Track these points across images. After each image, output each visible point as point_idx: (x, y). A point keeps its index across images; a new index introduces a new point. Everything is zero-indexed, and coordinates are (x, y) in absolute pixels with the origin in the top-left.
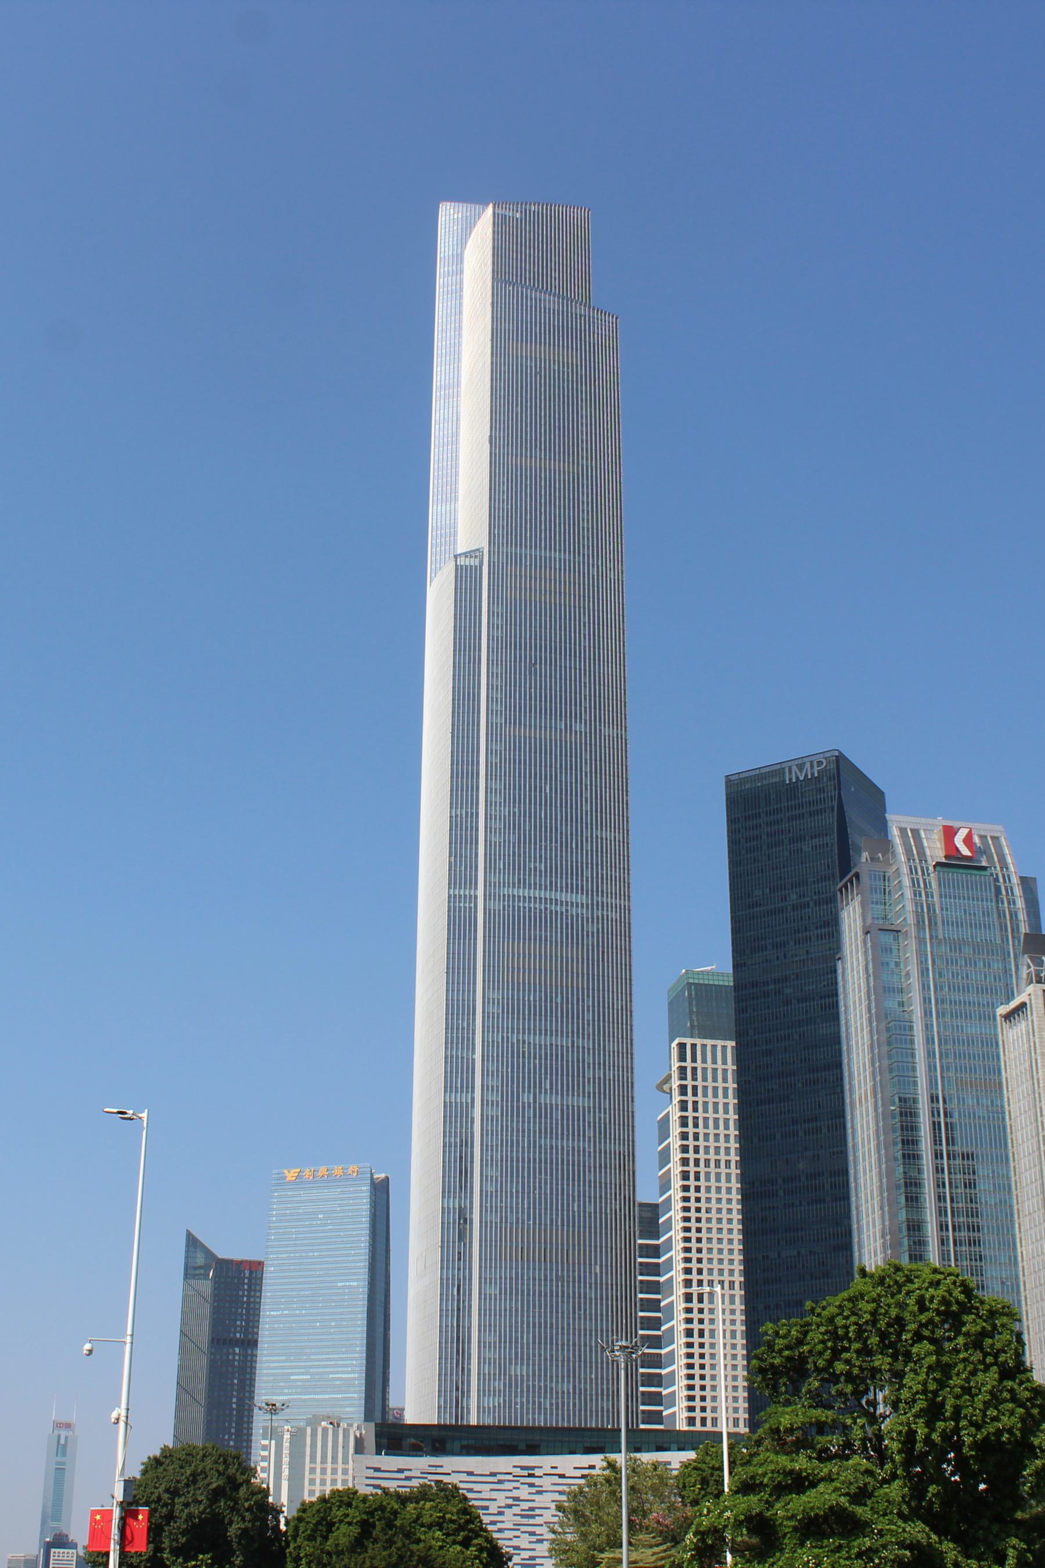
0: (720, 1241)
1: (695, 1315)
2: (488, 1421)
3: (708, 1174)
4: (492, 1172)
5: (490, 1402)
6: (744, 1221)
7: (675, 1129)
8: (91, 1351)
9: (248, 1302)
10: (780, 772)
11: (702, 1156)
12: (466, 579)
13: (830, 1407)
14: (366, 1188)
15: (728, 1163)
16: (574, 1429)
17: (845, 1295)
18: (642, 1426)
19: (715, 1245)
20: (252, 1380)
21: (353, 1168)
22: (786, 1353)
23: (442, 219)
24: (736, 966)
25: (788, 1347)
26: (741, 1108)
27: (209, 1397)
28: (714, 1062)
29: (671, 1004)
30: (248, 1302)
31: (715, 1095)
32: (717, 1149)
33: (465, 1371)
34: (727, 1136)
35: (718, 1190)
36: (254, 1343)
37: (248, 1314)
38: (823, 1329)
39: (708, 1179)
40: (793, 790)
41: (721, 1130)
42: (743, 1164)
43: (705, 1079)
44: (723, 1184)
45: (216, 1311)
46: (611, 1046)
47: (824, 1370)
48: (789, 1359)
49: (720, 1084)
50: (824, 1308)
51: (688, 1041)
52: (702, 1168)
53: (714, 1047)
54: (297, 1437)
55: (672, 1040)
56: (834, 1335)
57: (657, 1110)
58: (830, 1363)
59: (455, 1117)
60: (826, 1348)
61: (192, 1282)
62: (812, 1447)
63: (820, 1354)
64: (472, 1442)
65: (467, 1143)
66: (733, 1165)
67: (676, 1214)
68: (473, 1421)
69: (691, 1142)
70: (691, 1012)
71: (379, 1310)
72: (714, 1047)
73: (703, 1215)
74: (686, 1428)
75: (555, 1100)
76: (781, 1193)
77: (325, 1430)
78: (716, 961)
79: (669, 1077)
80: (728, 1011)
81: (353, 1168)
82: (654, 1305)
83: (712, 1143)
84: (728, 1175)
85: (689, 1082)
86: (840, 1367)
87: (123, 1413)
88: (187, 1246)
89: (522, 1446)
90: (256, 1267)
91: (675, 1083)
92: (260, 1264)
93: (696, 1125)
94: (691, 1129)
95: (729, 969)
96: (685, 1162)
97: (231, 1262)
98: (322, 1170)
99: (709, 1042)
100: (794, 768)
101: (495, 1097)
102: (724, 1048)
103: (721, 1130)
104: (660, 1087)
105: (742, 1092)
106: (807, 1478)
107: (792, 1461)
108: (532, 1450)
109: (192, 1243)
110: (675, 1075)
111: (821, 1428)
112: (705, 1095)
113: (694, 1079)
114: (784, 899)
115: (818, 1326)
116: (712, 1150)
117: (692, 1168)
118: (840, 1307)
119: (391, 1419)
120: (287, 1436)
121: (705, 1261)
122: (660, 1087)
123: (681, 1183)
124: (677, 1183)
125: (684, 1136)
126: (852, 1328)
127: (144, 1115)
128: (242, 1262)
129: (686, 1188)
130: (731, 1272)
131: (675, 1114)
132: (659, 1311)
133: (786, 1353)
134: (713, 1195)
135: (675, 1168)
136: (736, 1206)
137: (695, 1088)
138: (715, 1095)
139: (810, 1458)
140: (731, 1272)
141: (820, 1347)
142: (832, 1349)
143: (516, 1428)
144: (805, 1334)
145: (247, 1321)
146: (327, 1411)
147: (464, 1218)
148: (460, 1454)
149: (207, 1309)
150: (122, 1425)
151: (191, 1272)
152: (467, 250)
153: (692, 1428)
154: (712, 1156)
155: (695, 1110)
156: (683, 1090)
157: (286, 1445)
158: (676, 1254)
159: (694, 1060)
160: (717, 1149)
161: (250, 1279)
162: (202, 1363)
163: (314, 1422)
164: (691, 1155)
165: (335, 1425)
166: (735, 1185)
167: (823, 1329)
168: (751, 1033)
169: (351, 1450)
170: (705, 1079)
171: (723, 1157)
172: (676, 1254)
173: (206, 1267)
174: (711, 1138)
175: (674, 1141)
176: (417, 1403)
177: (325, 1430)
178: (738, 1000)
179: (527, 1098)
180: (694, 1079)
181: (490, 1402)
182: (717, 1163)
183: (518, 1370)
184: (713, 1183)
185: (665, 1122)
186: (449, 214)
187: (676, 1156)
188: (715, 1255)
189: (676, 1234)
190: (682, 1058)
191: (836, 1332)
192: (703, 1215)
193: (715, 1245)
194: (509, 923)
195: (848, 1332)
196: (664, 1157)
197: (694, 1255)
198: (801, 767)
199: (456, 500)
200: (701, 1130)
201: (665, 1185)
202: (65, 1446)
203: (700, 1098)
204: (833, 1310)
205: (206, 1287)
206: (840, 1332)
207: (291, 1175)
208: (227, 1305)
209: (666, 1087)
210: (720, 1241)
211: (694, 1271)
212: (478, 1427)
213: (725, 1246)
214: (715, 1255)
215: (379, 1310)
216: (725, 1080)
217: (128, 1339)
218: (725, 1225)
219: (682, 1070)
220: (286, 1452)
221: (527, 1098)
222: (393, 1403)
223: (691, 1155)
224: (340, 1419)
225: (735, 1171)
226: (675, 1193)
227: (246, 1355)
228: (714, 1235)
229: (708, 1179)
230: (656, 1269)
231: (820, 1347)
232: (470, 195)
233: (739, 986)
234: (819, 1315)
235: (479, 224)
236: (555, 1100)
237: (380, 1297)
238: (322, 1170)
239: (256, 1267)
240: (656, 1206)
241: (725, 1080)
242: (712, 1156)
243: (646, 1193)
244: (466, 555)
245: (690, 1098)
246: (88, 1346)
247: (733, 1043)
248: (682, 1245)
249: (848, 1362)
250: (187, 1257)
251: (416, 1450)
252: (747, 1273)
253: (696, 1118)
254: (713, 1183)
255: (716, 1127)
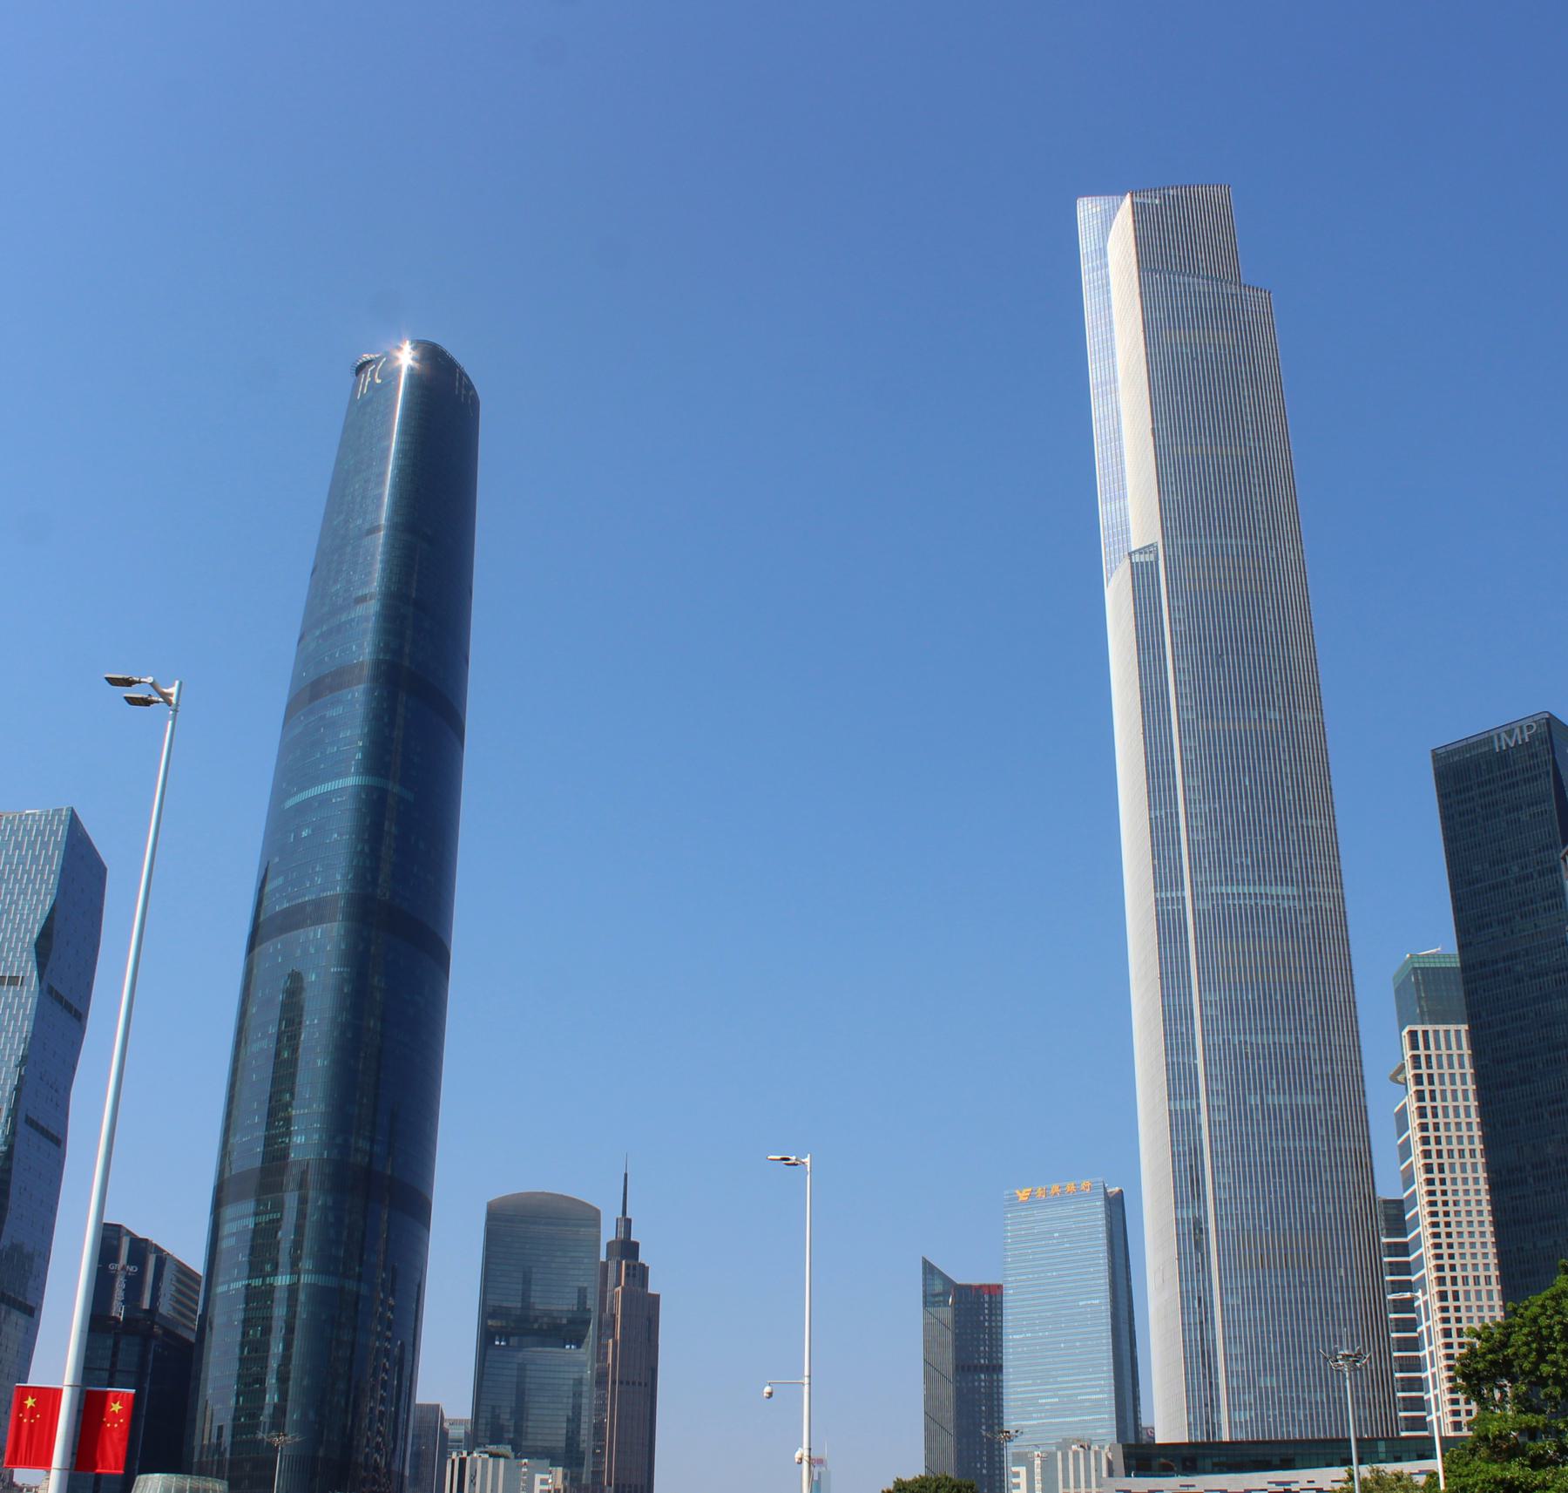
0: (1471, 1234)
1: (1452, 1314)
2: (1241, 1436)
3: (1452, 1166)
4: (1225, 1179)
5: (1242, 1416)
6: (1493, 1212)
7: (1414, 1121)
8: (770, 1394)
9: (990, 1327)
10: (1490, 740)
11: (1444, 1147)
12: (1142, 576)
13: (1539, 1411)
14: (1100, 1203)
15: (1472, 1152)
16: (1332, 1440)
17: (1547, 1293)
18: (1403, 1434)
19: (1466, 1239)
20: (1000, 1406)
21: (1085, 1184)
22: (1490, 1357)
23: (1080, 215)
24: (1461, 947)
25: (1491, 1351)
26: (1480, 1094)
27: (957, 1426)
28: (1449, 1047)
29: (1398, 992)
30: (990, 1327)
31: (1453, 1082)
32: (1460, 1138)
33: (1213, 1385)
34: (1469, 1125)
35: (1465, 1181)
36: (999, 1369)
37: (991, 1339)
38: (1525, 1330)
39: (1452, 1170)
40: (1504, 757)
41: (1463, 1119)
42: (1487, 1152)
43: (1440, 1066)
44: (1470, 1174)
45: (958, 1337)
46: (1336, 1040)
47: (1531, 1372)
48: (1493, 1363)
49: (1457, 1070)
50: (1526, 1308)
51: (1419, 1028)
52: (1445, 1160)
53: (1447, 1032)
54: (1049, 1462)
55: (1402, 1029)
56: (1538, 1336)
57: (1391, 1102)
58: (1536, 1365)
59: (1181, 1124)
60: (1530, 1352)
61: (931, 1310)
62: (1524, 1454)
63: (1526, 1356)
64: (1223, 1459)
65: (1197, 1152)
66: (1478, 1153)
67: (1422, 1209)
68: (1226, 1437)
69: (1431, 1133)
70: (1419, 998)
71: (1125, 1328)
72: (1447, 1032)
73: (1451, 1208)
74: (1452, 1434)
75: (1283, 1100)
76: (1531, 1180)
77: (1076, 1454)
78: (1440, 943)
79: (1403, 1067)
80: (1457, 995)
81: (1085, 1184)
82: (1408, 1306)
83: (1453, 1133)
84: (1474, 1165)
85: (1424, 1071)
86: (1546, 1369)
87: (806, 1453)
88: (925, 1273)
89: (1276, 1461)
90: (995, 1291)
91: (1410, 1073)
92: (1000, 1287)
93: (1435, 1115)
94: (1430, 1120)
95: (1455, 950)
96: (1427, 1154)
97: (970, 1287)
98: (1055, 1188)
99: (1441, 1028)
100: (1503, 736)
101: (1222, 1102)
102: (1458, 1032)
103: (1463, 1119)
104: (1394, 1078)
105: (1479, 1078)
106: (1519, 1487)
107: (1504, 1469)
108: (1287, 1464)
109: (929, 1269)
110: (1409, 1065)
111: (1532, 1433)
112: (1442, 1083)
113: (1429, 1066)
114: (1505, 872)
115: (1521, 1328)
116: (1454, 1140)
117: (1434, 1161)
118: (1543, 1306)
119: (1144, 1438)
120: (1038, 1462)
121: (1457, 1257)
122: (1394, 1078)
123: (1425, 1176)
124: (1420, 1176)
125: (1424, 1127)
126: (1557, 1328)
127: (807, 1160)
128: (981, 1287)
129: (1430, 1182)
130: (1486, 1266)
131: (1413, 1106)
132: (1413, 1311)
133: (1490, 1357)
134: (1460, 1187)
135: (1417, 1161)
136: (1485, 1197)
137: (1430, 1076)
138: (1453, 1082)
139: (1523, 1465)
140: (1486, 1266)
141: (1524, 1349)
142: (1537, 1350)
143: (1270, 1442)
144: (1508, 1335)
145: (991, 1347)
146: (1079, 1434)
147: (1199, 1227)
148: (1212, 1472)
149: (949, 1337)
150: (805, 1464)
151: (930, 1300)
152: (1109, 240)
153: (1458, 1434)
154: (1455, 1146)
155: (1433, 1099)
156: (1418, 1079)
157: (1038, 1470)
158: (1426, 1250)
159: (1427, 1047)
160: (1460, 1138)
161: (990, 1303)
162: (948, 1391)
163: (1064, 1446)
164: (1433, 1147)
165: (1086, 1448)
166: (1482, 1174)
167: (1525, 1330)
168: (1484, 1014)
169: (1105, 1474)
170: (1440, 1066)
171: (1466, 1146)
172: (1426, 1250)
173: (945, 1294)
174: (1453, 1127)
175: (1414, 1134)
176: (1167, 1422)
177: (1076, 1454)
178: (1466, 982)
179: (1254, 1100)
180: (1429, 1066)
181: (1242, 1416)
182: (1461, 1152)
183: (1268, 1382)
184: (1458, 1174)
185: (1402, 1114)
186: (1087, 210)
187: (1417, 1148)
188: (1467, 1250)
189: (1424, 1230)
190: (1414, 1046)
191: (1540, 1332)
192: (1451, 1208)
193: (1466, 1239)
194: (1217, 922)
195: (1552, 1333)
196: (1405, 1150)
197: (1445, 1251)
198: (1510, 733)
199: (1125, 496)
200: (1441, 1120)
201: (1408, 1180)
202: (818, 1482)
203: (1437, 1087)
204: (1535, 1310)
205: (946, 1314)
206: (1545, 1332)
207: (1023, 1195)
208: (970, 1330)
209: (1400, 1078)
210: (1471, 1234)
211: (1447, 1268)
212: (1231, 1443)
213: (1477, 1239)
214: (1467, 1250)
215: (1125, 1328)
216: (1462, 1066)
217: (806, 1380)
218: (1475, 1218)
219: (1416, 1059)
220: (1038, 1477)
221: (1254, 1100)
222: (1144, 1423)
223: (1433, 1147)
224: (1091, 1442)
225: (1480, 1160)
226: (1420, 1187)
227: (991, 1382)
228: (1465, 1228)
229: (1452, 1170)
230: (1406, 1268)
231: (1524, 1349)
232: (1107, 187)
233: (1466, 967)
234: (1521, 1316)
235: (1119, 215)
236: (1283, 1100)
237: (1124, 1314)
238: (1055, 1188)
239: (995, 1291)
240: (1401, 1202)
241: (1462, 1066)
242: (1455, 1146)
243: (1387, 1188)
244: (1140, 551)
245: (1426, 1087)
246: (767, 1389)
247: (1464, 1028)
248: (1431, 1241)
249: (1554, 1363)
250: (925, 1285)
251: (1166, 1471)
252: (1501, 1266)
253: (1434, 1108)
254: (1458, 1174)
255: (1457, 1115)
